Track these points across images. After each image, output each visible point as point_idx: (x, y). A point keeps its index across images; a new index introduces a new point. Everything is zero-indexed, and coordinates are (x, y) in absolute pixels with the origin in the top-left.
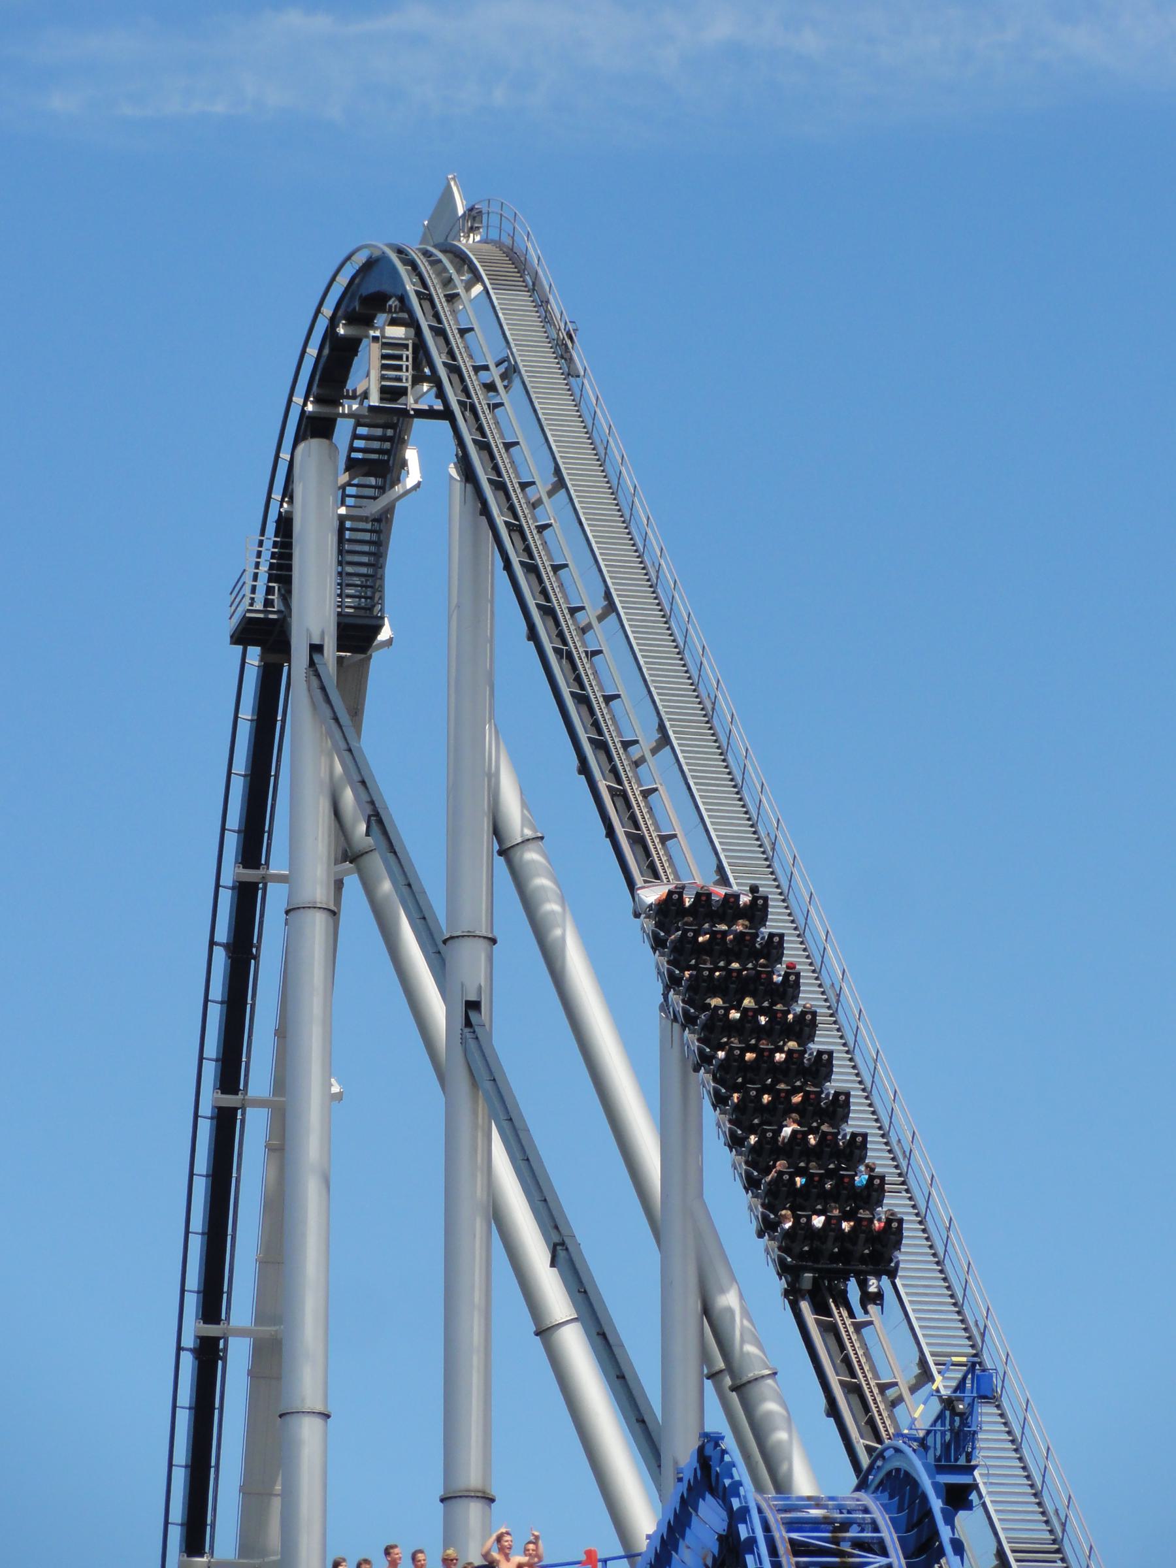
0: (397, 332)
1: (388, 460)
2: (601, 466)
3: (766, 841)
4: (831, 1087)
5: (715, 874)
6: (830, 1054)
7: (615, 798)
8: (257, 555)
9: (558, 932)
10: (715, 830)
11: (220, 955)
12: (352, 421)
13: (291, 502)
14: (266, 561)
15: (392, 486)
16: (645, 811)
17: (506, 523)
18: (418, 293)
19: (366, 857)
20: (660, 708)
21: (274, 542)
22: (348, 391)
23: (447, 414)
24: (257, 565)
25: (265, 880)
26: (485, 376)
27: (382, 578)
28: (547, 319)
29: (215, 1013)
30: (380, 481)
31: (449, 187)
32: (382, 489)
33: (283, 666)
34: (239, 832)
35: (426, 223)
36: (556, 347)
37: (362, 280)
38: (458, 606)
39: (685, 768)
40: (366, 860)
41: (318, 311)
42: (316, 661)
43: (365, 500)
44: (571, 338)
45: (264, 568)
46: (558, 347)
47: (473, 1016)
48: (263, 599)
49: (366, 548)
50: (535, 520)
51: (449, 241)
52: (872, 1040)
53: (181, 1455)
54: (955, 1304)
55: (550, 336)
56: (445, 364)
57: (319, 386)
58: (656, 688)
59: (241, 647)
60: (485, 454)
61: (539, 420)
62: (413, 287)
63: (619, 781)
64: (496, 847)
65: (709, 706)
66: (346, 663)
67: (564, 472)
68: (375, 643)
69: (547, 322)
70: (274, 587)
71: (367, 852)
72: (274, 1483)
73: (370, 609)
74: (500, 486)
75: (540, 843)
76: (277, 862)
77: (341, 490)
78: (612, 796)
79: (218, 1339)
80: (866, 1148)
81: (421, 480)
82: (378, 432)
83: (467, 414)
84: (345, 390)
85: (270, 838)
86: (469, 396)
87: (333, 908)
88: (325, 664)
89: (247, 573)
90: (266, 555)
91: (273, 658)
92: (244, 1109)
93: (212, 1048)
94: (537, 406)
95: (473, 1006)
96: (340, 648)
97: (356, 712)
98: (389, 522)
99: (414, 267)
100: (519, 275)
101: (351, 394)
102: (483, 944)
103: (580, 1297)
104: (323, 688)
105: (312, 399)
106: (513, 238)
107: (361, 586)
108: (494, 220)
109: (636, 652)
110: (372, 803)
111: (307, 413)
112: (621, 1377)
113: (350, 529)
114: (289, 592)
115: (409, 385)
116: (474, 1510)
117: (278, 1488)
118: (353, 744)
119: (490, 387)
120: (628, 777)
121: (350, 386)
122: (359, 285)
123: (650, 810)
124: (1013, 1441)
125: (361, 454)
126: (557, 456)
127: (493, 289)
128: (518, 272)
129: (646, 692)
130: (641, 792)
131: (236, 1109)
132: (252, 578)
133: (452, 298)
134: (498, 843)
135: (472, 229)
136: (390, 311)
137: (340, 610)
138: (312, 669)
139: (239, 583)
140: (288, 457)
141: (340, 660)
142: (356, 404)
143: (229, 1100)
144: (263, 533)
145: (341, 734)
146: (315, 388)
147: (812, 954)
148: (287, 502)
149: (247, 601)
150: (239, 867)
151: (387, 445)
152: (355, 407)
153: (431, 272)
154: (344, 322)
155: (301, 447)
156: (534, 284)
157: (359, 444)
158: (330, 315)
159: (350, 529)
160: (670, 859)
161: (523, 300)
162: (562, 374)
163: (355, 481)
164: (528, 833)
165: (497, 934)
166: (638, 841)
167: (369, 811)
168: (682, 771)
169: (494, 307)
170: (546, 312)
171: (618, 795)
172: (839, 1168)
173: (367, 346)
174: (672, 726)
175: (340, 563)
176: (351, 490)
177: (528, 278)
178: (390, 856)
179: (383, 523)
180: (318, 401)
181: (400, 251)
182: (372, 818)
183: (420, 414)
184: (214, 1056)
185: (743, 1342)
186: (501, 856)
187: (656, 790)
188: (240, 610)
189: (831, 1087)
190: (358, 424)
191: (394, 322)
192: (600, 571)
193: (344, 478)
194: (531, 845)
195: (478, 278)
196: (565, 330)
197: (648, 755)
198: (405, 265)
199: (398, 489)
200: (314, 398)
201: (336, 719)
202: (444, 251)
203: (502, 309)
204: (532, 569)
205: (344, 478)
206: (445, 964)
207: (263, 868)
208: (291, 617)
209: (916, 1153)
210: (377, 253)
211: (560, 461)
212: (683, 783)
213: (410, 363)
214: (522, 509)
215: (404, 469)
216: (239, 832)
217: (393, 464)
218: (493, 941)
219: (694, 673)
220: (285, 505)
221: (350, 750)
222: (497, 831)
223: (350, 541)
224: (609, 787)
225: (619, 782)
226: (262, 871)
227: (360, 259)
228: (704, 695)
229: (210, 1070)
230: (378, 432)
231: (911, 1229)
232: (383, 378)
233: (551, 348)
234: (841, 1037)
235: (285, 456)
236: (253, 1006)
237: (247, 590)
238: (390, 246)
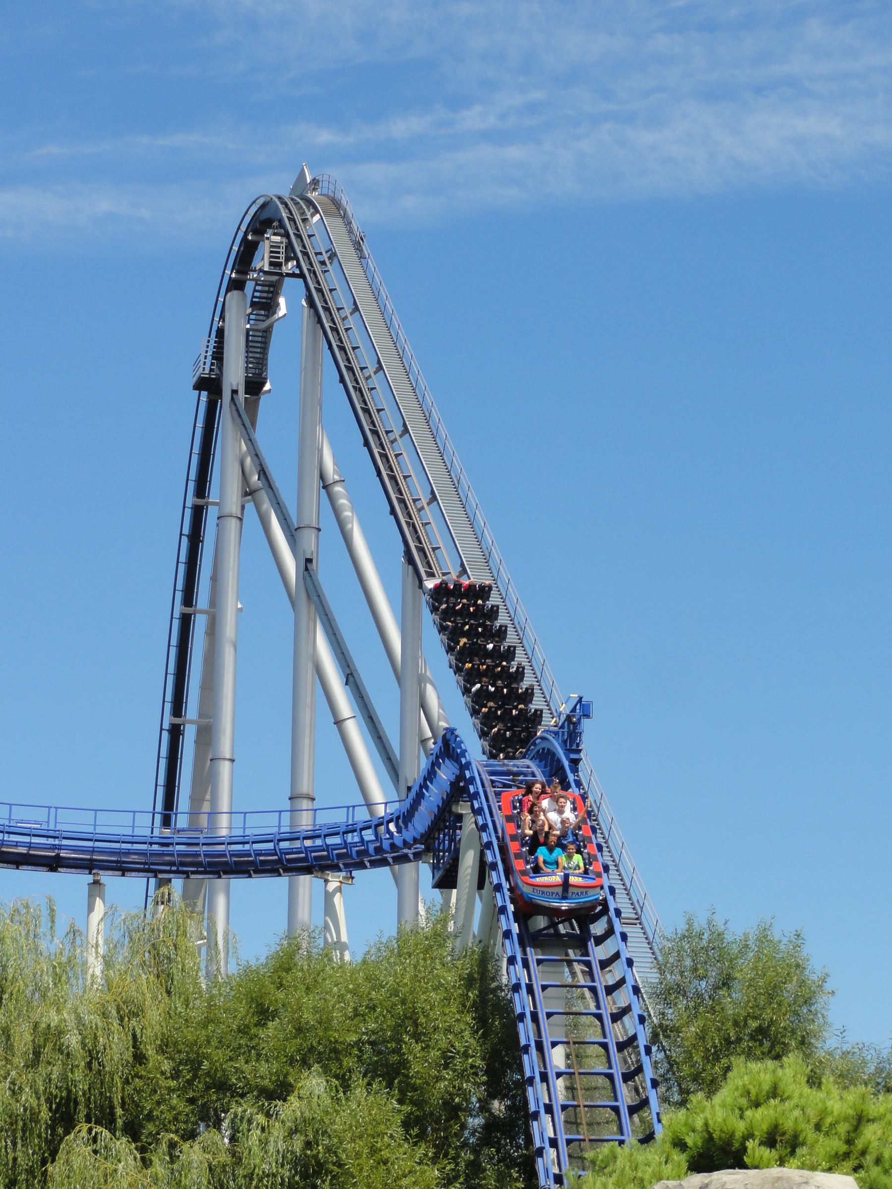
0: (277, 239)
3: (455, 479)
4: (533, 707)
6: (498, 607)
9: (350, 526)
11: (185, 540)
12: (254, 283)
13: (224, 321)
16: (396, 463)
17: (330, 326)
23: (302, 276)
24: (207, 352)
25: (207, 504)
26: (320, 258)
27: (267, 359)
28: (350, 232)
29: (182, 568)
30: (266, 312)
31: (303, 169)
32: (268, 317)
34: (182, 591)
38: (305, 368)
39: (416, 444)
40: (257, 494)
41: (239, 228)
44: (362, 239)
45: (210, 353)
47: (309, 566)
49: (259, 345)
50: (344, 326)
51: (304, 194)
52: (506, 573)
53: (162, 780)
54: (546, 701)
56: (301, 251)
57: (239, 265)
60: (320, 294)
61: (346, 279)
63: (384, 449)
64: (322, 485)
65: (428, 415)
67: (358, 303)
72: (205, 795)
73: (261, 374)
74: (327, 309)
76: (214, 495)
79: (180, 725)
80: (542, 717)
82: (266, 289)
83: (312, 275)
85: (210, 484)
86: (312, 266)
87: (239, 516)
90: (211, 347)
91: (214, 397)
92: (195, 614)
93: (180, 585)
94: (345, 272)
95: (309, 561)
97: (253, 424)
98: (271, 333)
99: (286, 205)
102: (315, 531)
103: (359, 699)
104: (238, 411)
107: (256, 363)
108: (325, 184)
110: (261, 465)
112: (380, 738)
113: (252, 336)
114: (222, 365)
115: (283, 261)
116: (305, 804)
117: (208, 797)
119: (323, 263)
121: (253, 265)
122: (259, 215)
123: (399, 464)
124: (625, 889)
126: (355, 295)
129: (397, 408)
131: (191, 615)
133: (305, 220)
135: (314, 189)
136: (274, 228)
139: (197, 361)
140: (222, 300)
141: (246, 398)
143: (188, 610)
144: (209, 337)
146: (236, 267)
149: (201, 369)
151: (270, 295)
155: (229, 294)
157: (257, 294)
159: (252, 336)
160: (408, 487)
163: (254, 313)
164: (337, 478)
165: (321, 527)
166: (393, 478)
167: (259, 468)
169: (325, 225)
172: (484, 622)
175: (247, 352)
176: (252, 317)
177: (341, 212)
178: (270, 490)
180: (237, 272)
181: (279, 198)
183: (288, 275)
185: (439, 720)
187: (401, 454)
188: (198, 374)
189: (533, 707)
190: (257, 284)
191: (275, 234)
192: (375, 350)
193: (249, 310)
194: (338, 484)
195: (317, 211)
197: (372, 375)
199: (276, 317)
201: (244, 425)
202: (301, 199)
204: (342, 349)
206: (295, 541)
209: (527, 628)
210: (268, 199)
211: (356, 298)
213: (284, 250)
214: (337, 319)
216: (195, 481)
218: (319, 530)
219: (421, 399)
221: (250, 440)
222: (322, 477)
223: (252, 341)
225: (384, 449)
226: (205, 500)
227: (261, 201)
228: (425, 410)
229: (179, 596)
230: (266, 289)
231: (537, 691)
232: (271, 257)
234: (534, 674)
235: (221, 299)
236: (186, 703)
237: (202, 363)
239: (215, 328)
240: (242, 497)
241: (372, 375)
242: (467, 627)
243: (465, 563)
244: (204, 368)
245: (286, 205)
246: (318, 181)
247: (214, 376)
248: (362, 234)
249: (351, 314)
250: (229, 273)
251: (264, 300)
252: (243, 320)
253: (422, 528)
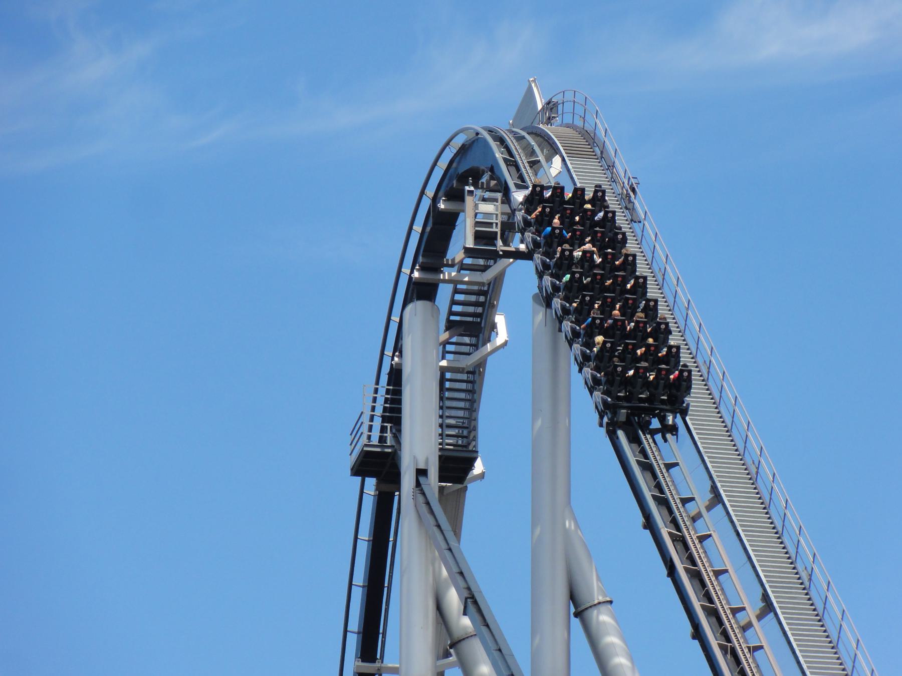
1: (480, 323)
2: (659, 289)
5: (760, 602)
7: (675, 543)
8: (372, 409)
10: (761, 566)
12: (450, 287)
13: (401, 356)
14: (382, 396)
15: (484, 344)
16: (701, 551)
18: (505, 160)
19: (463, 643)
20: (712, 472)
21: (387, 389)
22: (447, 260)
24: (373, 409)
30: (474, 340)
32: (476, 346)
33: (394, 495)
34: (358, 633)
35: (511, 122)
36: (621, 200)
37: (459, 163)
39: (734, 519)
40: (464, 645)
41: (422, 193)
42: (421, 482)
43: (463, 347)
44: (633, 190)
45: (379, 411)
46: (622, 200)
48: (380, 426)
55: (616, 192)
58: (709, 457)
59: (359, 479)
62: (501, 155)
63: (678, 528)
64: (573, 610)
65: (754, 470)
66: (445, 492)
68: (469, 476)
69: (613, 182)
70: (387, 426)
71: (464, 639)
75: (609, 606)
77: (442, 346)
78: (673, 541)
81: (507, 339)
82: (473, 298)
84: (445, 259)
88: (429, 485)
89: (364, 425)
91: (386, 488)
96: (441, 479)
97: (457, 530)
98: (482, 375)
99: (501, 141)
100: (589, 147)
101: (450, 263)
104: (428, 503)
105: (417, 267)
106: (584, 118)
108: (568, 107)
109: (692, 430)
110: (469, 589)
111: (414, 279)
113: (450, 380)
115: (498, 230)
118: (453, 543)
120: (686, 525)
125: (459, 317)
127: (568, 157)
128: (589, 145)
129: (700, 461)
130: (698, 537)
132: (368, 420)
134: (575, 607)
137: (441, 446)
138: (418, 489)
139: (358, 423)
140: (398, 320)
141: (441, 489)
142: (454, 272)
144: (377, 383)
145: (443, 538)
146: (420, 259)
147: (845, 662)
148: (398, 357)
149: (364, 437)
150: (358, 661)
151: (480, 310)
152: (453, 274)
153: (518, 147)
154: (444, 198)
156: (602, 153)
157: (457, 308)
158: (432, 196)
159: (450, 380)
161: (594, 165)
162: (627, 220)
163: (454, 340)
164: (601, 599)
166: (696, 576)
167: (466, 594)
168: (732, 522)
170: (612, 173)
171: (678, 541)
173: (462, 222)
174: (722, 486)
175: (441, 408)
176: (450, 348)
179: (477, 375)
180: (423, 269)
181: (490, 131)
182: (469, 600)
184: (356, 630)
186: (577, 618)
187: (710, 536)
190: (456, 291)
193: (444, 336)
194: (603, 608)
195: (556, 151)
196: (628, 184)
197: (704, 511)
198: (495, 141)
199: (489, 347)
200: (419, 266)
201: (439, 526)
203: (575, 171)
205: (444, 336)
207: (379, 662)
208: (400, 450)
212: (733, 531)
215: (494, 331)
217: (485, 324)
220: (396, 359)
221: (450, 550)
223: (449, 390)
224: (670, 533)
226: (377, 665)
233: (617, 201)
235: (395, 318)
237: (365, 428)
238: (485, 128)
239: (386, 369)
240: (438, 659)
241: (704, 511)
242: (631, 372)
243: (771, 595)
244: (369, 437)
245: (501, 141)
246: (556, 105)
247: (390, 450)
248: (632, 180)
249: (760, 617)
250: (408, 272)
251: (470, 319)
252: (436, 351)
253: (748, 656)
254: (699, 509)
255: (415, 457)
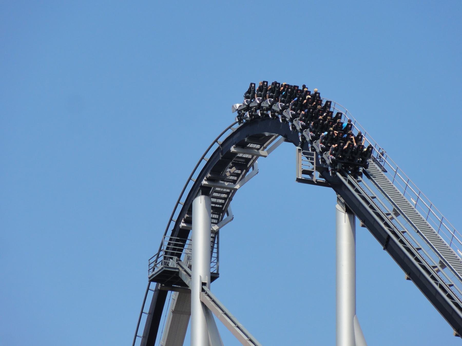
144: (165, 234)
254: (298, 154)
255: (191, 270)
